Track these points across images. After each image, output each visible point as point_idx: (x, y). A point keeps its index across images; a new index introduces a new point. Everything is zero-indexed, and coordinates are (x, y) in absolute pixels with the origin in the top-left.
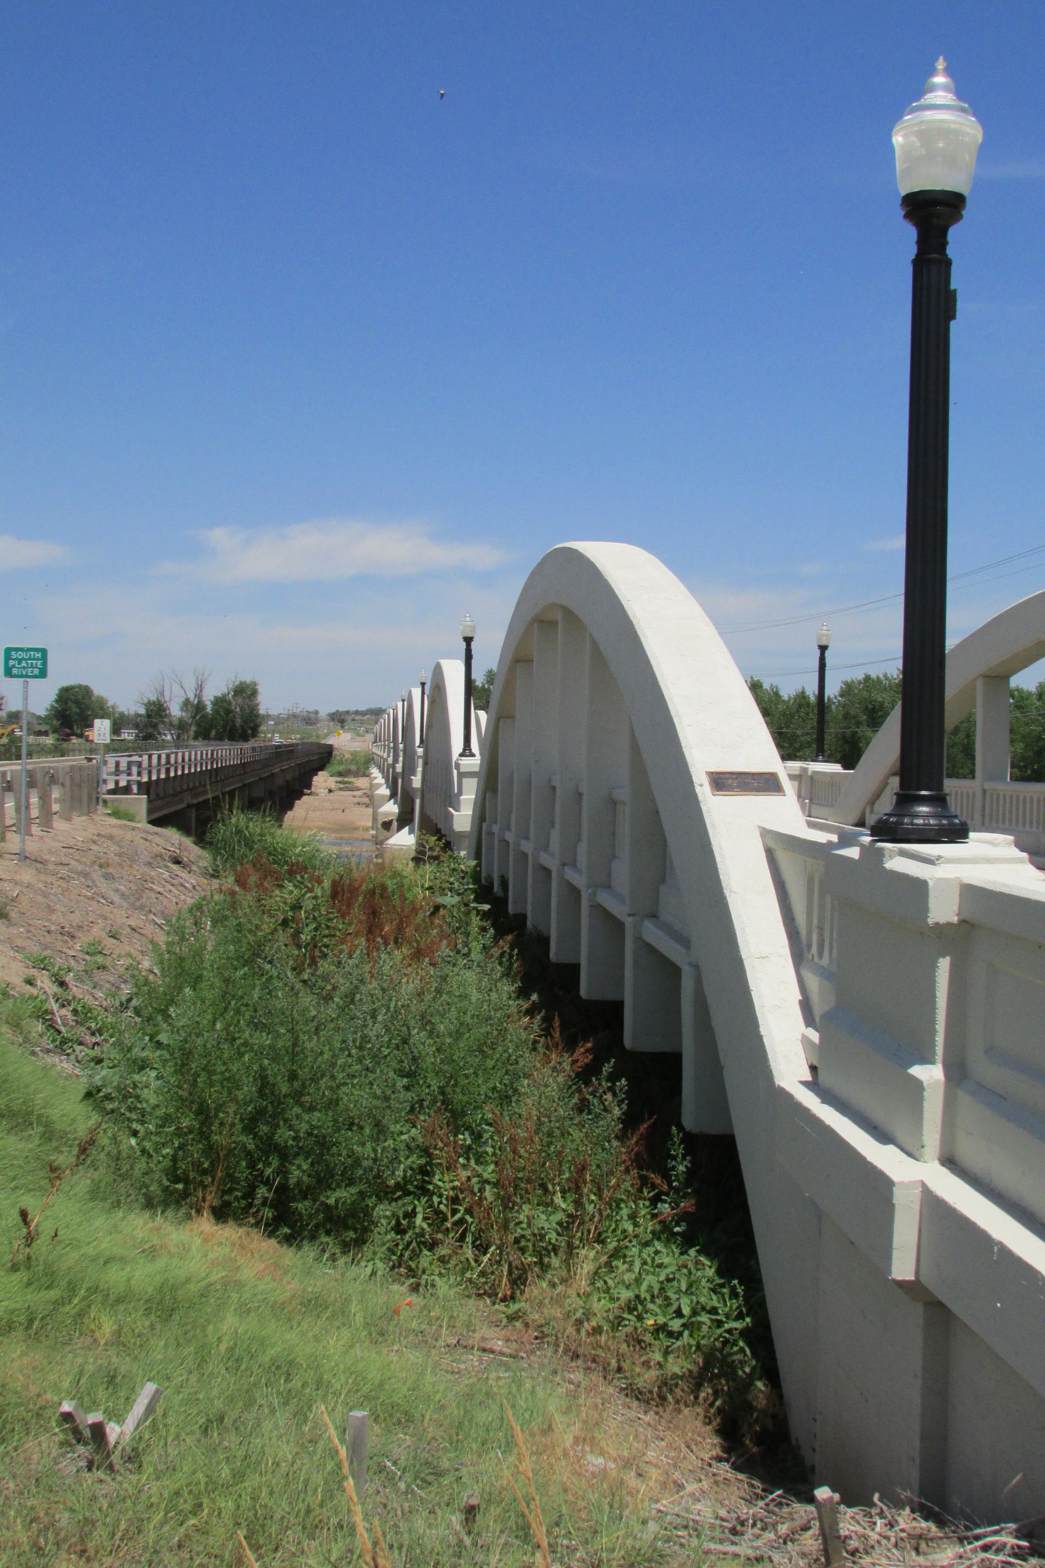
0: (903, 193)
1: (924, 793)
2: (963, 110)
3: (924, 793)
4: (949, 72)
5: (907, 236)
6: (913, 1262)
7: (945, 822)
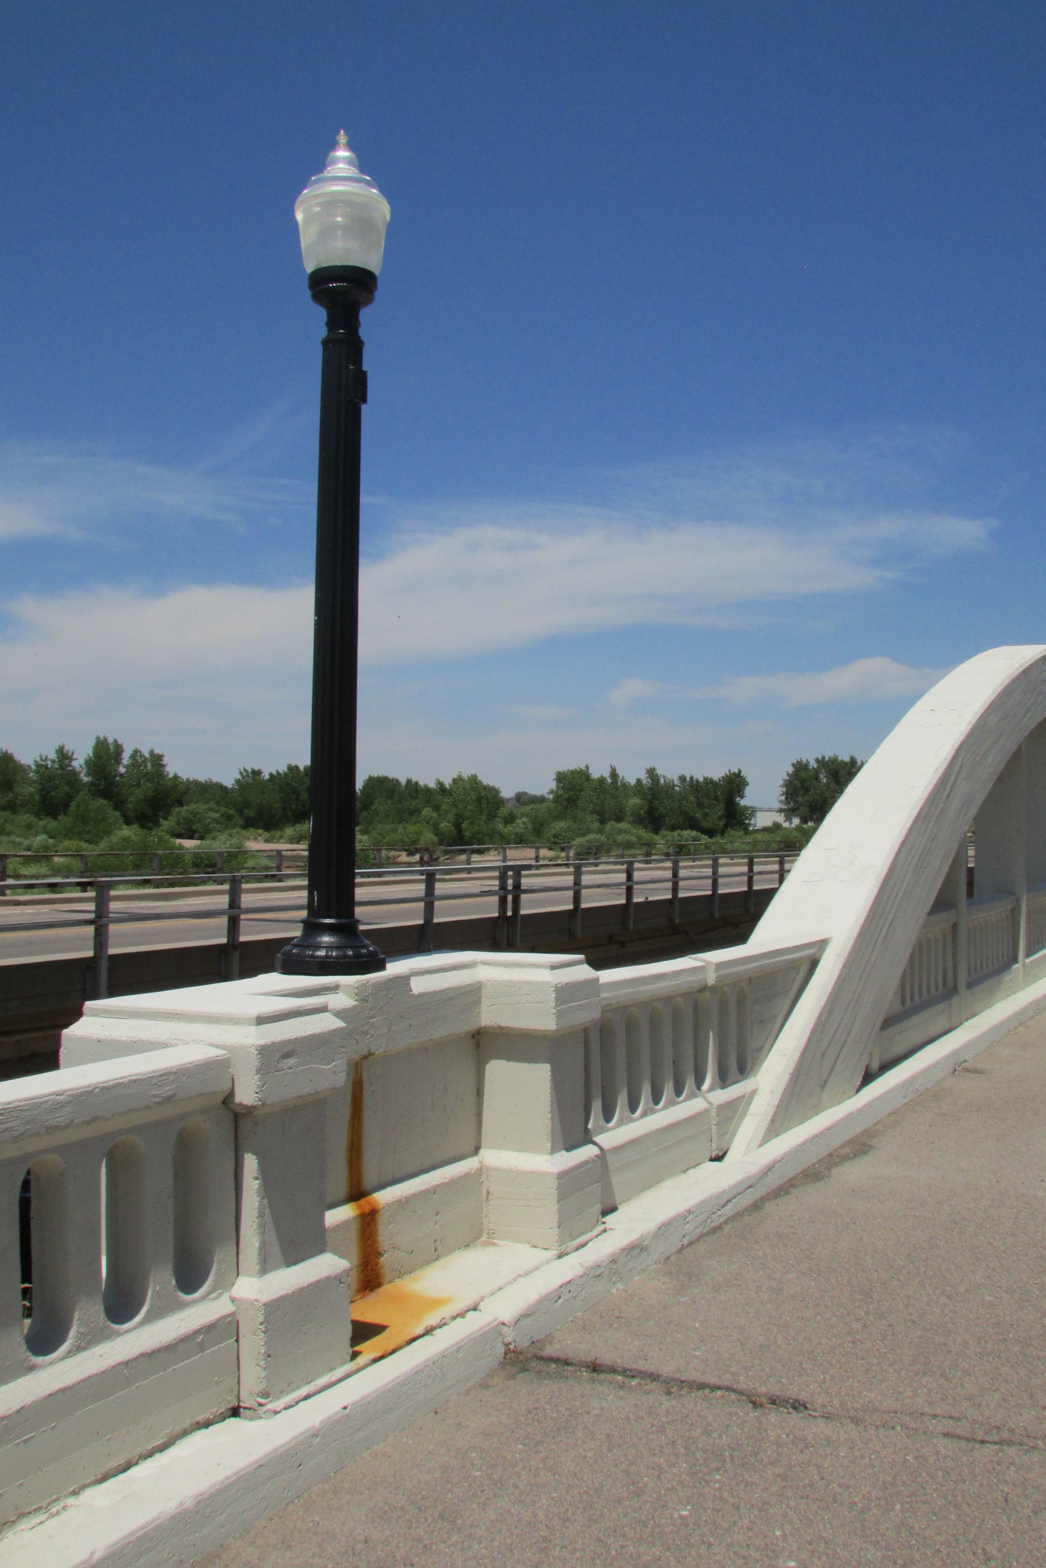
0: (310, 267)
1: (328, 921)
2: (368, 184)
3: (328, 921)
4: (351, 146)
5: (316, 321)
6: (788, 1024)
7: (350, 953)
